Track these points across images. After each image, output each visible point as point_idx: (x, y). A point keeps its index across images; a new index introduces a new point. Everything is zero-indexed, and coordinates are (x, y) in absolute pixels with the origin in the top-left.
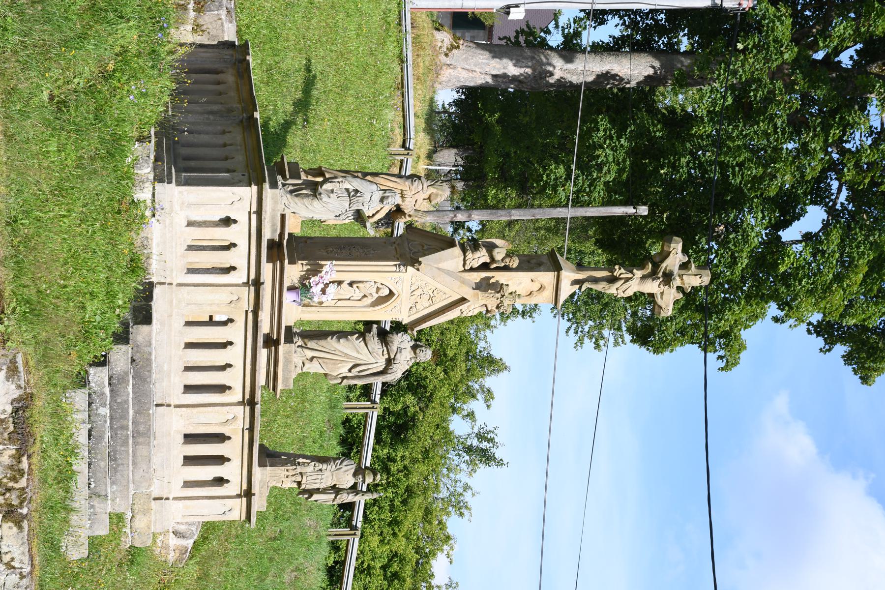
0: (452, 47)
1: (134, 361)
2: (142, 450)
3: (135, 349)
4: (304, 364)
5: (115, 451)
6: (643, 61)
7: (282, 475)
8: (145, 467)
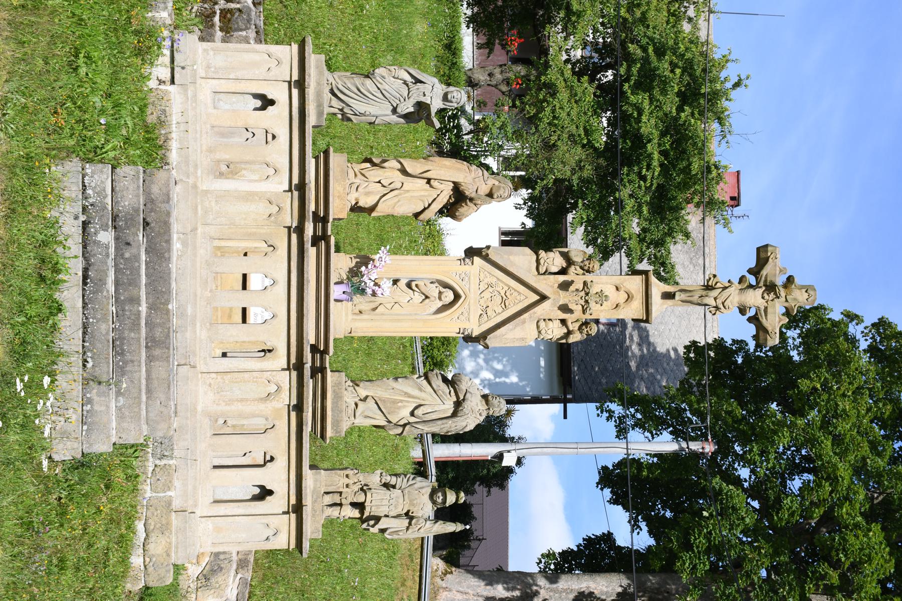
0: (445, 573)
1: (148, 224)
2: (159, 370)
3: (148, 205)
4: (356, 405)
5: (122, 339)
6: (615, 579)
7: (341, 484)
8: (162, 397)
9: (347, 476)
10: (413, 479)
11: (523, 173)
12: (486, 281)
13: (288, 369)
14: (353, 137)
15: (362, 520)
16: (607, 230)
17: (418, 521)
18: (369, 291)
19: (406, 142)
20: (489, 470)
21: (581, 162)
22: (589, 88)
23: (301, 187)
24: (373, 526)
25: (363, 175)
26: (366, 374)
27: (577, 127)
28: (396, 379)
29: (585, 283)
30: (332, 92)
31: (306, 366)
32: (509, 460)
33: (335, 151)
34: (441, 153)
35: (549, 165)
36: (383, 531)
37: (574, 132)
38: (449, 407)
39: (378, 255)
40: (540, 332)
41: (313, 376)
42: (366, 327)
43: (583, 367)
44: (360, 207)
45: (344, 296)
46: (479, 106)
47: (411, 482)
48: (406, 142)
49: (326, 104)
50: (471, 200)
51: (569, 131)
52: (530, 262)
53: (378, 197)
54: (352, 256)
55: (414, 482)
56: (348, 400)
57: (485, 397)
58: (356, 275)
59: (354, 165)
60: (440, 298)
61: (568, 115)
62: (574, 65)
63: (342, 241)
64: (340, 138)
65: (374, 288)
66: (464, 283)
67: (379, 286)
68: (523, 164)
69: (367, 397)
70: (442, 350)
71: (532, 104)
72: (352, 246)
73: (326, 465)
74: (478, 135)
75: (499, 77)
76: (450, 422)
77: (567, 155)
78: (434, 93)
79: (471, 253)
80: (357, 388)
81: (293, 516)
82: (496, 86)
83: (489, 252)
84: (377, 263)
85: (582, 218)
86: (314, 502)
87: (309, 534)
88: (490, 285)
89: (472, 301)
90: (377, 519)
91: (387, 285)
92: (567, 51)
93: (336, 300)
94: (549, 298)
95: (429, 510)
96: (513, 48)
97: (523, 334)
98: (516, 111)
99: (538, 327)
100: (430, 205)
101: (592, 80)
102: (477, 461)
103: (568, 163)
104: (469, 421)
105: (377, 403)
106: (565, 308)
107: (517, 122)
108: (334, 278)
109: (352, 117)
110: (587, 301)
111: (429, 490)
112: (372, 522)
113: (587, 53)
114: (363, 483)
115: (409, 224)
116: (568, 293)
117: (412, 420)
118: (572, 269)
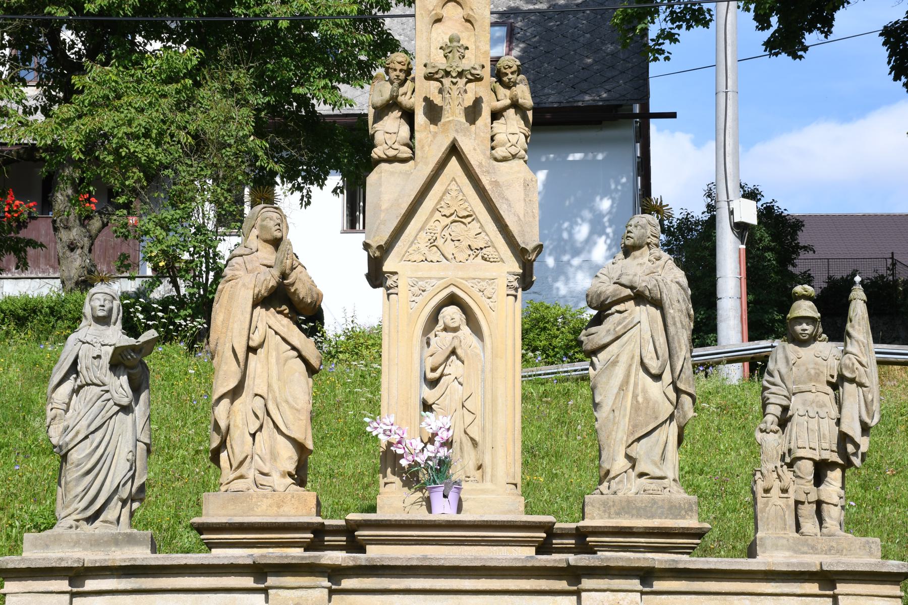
4: (641, 475)
7: (781, 502)
9: (767, 491)
10: (771, 375)
11: (247, 191)
12: (426, 250)
13: (578, 593)
14: (178, 484)
15: (847, 464)
16: (347, 44)
17: (847, 367)
18: (443, 452)
19: (189, 393)
20: (767, 249)
21: (224, 90)
22: (92, 74)
23: (260, 571)
24: (857, 446)
25: (241, 463)
26: (592, 461)
27: (164, 96)
28: (596, 405)
29: (429, 77)
30: (92, 519)
31: (572, 563)
32: (748, 212)
33: (199, 514)
34: (204, 334)
35: (230, 146)
36: (865, 429)
37: (171, 101)
38: (645, 314)
39: (381, 437)
40: (514, 156)
41: (591, 550)
42: (505, 455)
43: (584, 86)
44: (298, 469)
45: (452, 495)
46: (127, 267)
47: (777, 379)
48: (189, 393)
49: (113, 530)
50: (284, 276)
51: (171, 110)
52: (392, 173)
53: (280, 438)
54: (382, 481)
55: (776, 374)
56: (634, 490)
57: (628, 251)
58: (415, 474)
59: (223, 480)
60: (456, 330)
61: (141, 111)
62: (52, 100)
63: (359, 503)
64: (178, 508)
65: (437, 444)
66: (428, 288)
67: (435, 435)
68: (229, 191)
69: (628, 457)
70: (554, 331)
71: (123, 175)
72: (368, 486)
73: (750, 531)
74: (180, 270)
75: (75, 233)
76: (670, 312)
77: (212, 113)
78: (96, 341)
79: (376, 276)
80: (612, 475)
81: (841, 588)
82: (92, 238)
83: (374, 245)
84: (395, 438)
85: (325, 87)
86: (814, 550)
87: (873, 560)
88: (433, 244)
89: (460, 274)
90: (844, 438)
91: (432, 422)
92: (28, 111)
93: (459, 510)
94: (455, 140)
95: (825, 352)
96: (24, 208)
97: (521, 187)
98: (136, 204)
99: (505, 159)
100: (294, 348)
101: (78, 68)
102: (748, 269)
103: (226, 111)
104: (671, 279)
105: (639, 439)
106: (473, 113)
107: (156, 201)
108: (421, 514)
109: (138, 483)
110: (460, 74)
111: (791, 347)
112: (850, 448)
113: (31, 77)
114: (779, 464)
115: (333, 388)
116: (446, 107)
117: (667, 377)
118: (404, 100)
